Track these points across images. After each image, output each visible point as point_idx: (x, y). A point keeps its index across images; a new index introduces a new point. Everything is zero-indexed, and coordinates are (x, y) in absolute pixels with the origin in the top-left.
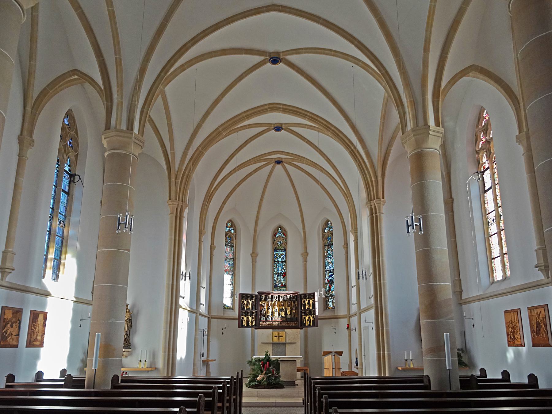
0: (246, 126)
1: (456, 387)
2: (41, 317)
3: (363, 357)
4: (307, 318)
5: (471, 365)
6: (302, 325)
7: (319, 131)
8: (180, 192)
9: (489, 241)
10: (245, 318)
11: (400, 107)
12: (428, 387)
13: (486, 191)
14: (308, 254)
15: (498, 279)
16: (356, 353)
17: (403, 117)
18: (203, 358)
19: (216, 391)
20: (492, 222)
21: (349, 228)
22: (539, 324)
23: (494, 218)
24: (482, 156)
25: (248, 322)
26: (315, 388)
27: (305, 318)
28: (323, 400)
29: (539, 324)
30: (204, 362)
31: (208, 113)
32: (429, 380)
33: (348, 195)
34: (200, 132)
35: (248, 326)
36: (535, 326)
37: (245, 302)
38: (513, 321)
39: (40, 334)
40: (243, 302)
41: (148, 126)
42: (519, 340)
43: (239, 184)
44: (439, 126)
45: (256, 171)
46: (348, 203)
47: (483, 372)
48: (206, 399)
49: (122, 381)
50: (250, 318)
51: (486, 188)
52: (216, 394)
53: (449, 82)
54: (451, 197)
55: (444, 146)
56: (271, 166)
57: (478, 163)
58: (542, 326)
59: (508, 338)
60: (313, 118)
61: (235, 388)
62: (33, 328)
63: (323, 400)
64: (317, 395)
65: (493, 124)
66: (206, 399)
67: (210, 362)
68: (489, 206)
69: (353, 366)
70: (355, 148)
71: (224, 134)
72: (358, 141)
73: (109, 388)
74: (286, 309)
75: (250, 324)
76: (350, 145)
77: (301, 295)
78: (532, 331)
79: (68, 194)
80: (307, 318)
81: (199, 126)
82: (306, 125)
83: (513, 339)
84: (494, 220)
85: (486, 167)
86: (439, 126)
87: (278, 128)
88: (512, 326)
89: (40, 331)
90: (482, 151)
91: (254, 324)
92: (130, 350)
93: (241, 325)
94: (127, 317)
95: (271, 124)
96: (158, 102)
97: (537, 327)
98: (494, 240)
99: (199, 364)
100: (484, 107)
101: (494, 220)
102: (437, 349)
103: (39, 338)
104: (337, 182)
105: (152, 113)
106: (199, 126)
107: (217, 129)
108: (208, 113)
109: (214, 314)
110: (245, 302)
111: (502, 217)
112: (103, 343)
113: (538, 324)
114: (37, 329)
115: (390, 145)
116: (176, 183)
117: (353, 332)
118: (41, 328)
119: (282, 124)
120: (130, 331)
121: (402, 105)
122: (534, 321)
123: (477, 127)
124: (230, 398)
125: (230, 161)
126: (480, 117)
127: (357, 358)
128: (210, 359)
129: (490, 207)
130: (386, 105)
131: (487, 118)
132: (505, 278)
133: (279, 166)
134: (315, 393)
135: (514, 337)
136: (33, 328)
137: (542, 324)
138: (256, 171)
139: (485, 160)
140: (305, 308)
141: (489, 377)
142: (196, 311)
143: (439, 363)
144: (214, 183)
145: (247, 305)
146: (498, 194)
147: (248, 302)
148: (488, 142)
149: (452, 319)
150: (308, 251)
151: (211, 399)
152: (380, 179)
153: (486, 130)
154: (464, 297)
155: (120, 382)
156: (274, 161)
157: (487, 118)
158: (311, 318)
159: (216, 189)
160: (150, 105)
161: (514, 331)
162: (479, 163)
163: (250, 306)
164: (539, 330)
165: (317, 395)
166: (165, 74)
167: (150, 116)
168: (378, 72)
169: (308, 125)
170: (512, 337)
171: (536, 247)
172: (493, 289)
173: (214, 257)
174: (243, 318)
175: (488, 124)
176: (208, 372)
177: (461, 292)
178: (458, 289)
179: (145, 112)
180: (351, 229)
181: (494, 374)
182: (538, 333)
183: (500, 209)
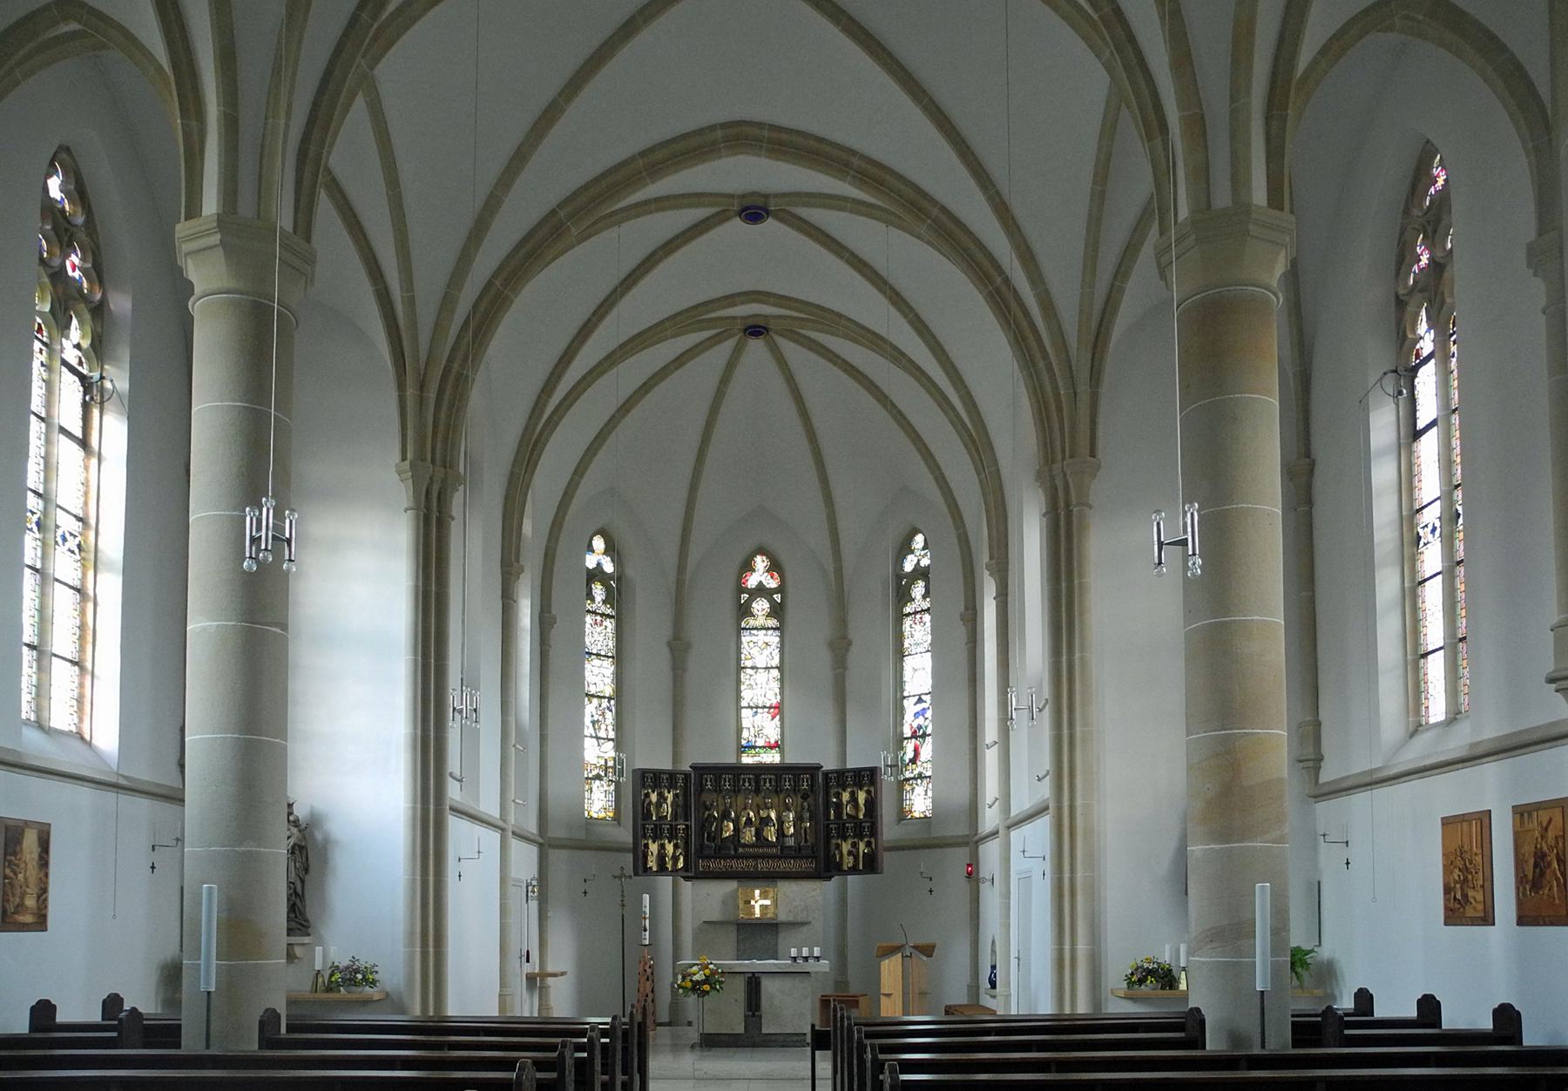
0: (647, 202)
1: (1280, 1040)
2: (30, 841)
3: (1014, 962)
4: (846, 847)
5: (1327, 973)
6: (826, 868)
7: (888, 223)
8: (435, 433)
9: (1417, 669)
10: (654, 847)
11: (1158, 141)
12: (1199, 1042)
13: (1417, 434)
14: (850, 643)
15: (1432, 721)
16: (993, 952)
17: (1163, 173)
18: (527, 968)
19: (567, 1054)
20: (1430, 537)
21: (983, 557)
22: (1544, 856)
23: (1438, 524)
24: (1418, 314)
25: (661, 857)
26: (862, 1049)
27: (838, 847)
28: (885, 1077)
29: (1544, 856)
30: (530, 979)
31: (519, 158)
32: (1203, 1022)
33: (979, 444)
34: (496, 226)
35: (662, 869)
36: (1532, 861)
37: (654, 797)
38: (1466, 848)
39: (32, 890)
40: (647, 795)
41: (324, 205)
42: (1480, 907)
43: (625, 408)
44: (1282, 209)
45: (680, 361)
46: (980, 468)
47: (1364, 999)
48: (539, 1075)
49: (290, 1029)
50: (670, 848)
51: (1421, 425)
52: (569, 1062)
53: (1324, 50)
54: (1308, 455)
55: (1293, 275)
56: (729, 344)
57: (1404, 340)
58: (1549, 864)
59: (1446, 900)
60: (872, 173)
61: (625, 1049)
62: (8, 871)
63: (885, 1077)
64: (869, 1065)
65: (1458, 205)
66: (539, 1075)
67: (550, 980)
68: (1423, 485)
69: (982, 991)
70: (1007, 281)
71: (574, 231)
72: (1016, 261)
73: (251, 1046)
74: (779, 817)
75: (669, 866)
76: (992, 271)
77: (826, 774)
78: (1521, 880)
79: (84, 443)
80: (846, 847)
81: (491, 205)
82: (846, 199)
83: (1464, 902)
84: (1434, 529)
85: (1425, 353)
86: (1282, 209)
87: (754, 212)
88: (1459, 863)
89: (32, 880)
90: (1418, 297)
91: (681, 865)
92: (306, 940)
93: (641, 867)
94: (292, 841)
95: (732, 196)
96: (356, 122)
97: (1536, 865)
98: (1433, 594)
99: (519, 985)
100: (1437, 143)
101: (1434, 529)
102: (1231, 933)
103: (30, 902)
104: (946, 398)
105: (339, 160)
106: (491, 205)
107: (553, 212)
108: (519, 158)
109: (556, 832)
110: (654, 797)
111: (1461, 521)
112: (224, 915)
113: (1540, 857)
114: (21, 876)
115: (1122, 271)
116: (421, 401)
117: (985, 888)
118: (32, 871)
119: (766, 196)
120: (303, 882)
121: (1164, 128)
122: (1528, 850)
123: (1406, 212)
124: (613, 1079)
125: (595, 326)
126: (1421, 175)
127: (994, 967)
128: (550, 969)
129: (1429, 485)
130: (1109, 128)
131: (1441, 182)
132: (1454, 715)
133: (756, 346)
134: (862, 1062)
135: (1465, 896)
136: (8, 871)
137: (1552, 857)
138: (680, 361)
139: (1422, 328)
140: (839, 814)
141: (1379, 1013)
142: (500, 823)
143: (1235, 973)
144: (545, 405)
145: (659, 805)
146: (1456, 443)
147: (660, 795)
148: (1437, 267)
149: (1281, 840)
150: (852, 635)
151: (554, 1075)
152: (1083, 389)
153: (1434, 223)
154: (1328, 774)
155: (283, 1030)
156: (739, 326)
157: (1441, 182)
158: (862, 846)
159: (552, 423)
160: (326, 130)
161: (1466, 880)
162: (1405, 336)
163: (667, 809)
164: (1542, 874)
165: (869, 1065)
166: (375, 17)
167: (328, 171)
168: (1090, 11)
169: (855, 201)
170: (1459, 896)
171: (1555, 618)
172: (1418, 752)
173: (553, 653)
174: (646, 846)
175: (1444, 197)
176: (543, 1004)
177: (1319, 759)
178: (1309, 752)
179: (311, 154)
180: (986, 559)
181: (1396, 1004)
182: (1536, 884)
183: (1458, 495)
